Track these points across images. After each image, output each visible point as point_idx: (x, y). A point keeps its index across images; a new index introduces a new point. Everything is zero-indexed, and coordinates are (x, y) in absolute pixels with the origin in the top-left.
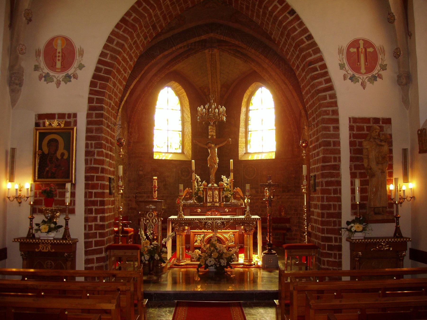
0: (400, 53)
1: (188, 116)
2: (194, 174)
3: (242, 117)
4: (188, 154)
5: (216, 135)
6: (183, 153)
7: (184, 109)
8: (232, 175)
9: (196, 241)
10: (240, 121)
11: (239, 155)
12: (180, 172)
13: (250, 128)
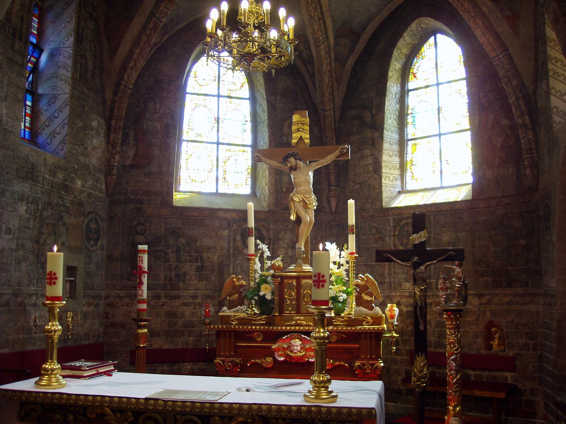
2: (252, 241)
3: (391, 106)
4: (262, 197)
5: (311, 138)
7: (258, 95)
8: (352, 238)
10: (384, 113)
11: (384, 195)
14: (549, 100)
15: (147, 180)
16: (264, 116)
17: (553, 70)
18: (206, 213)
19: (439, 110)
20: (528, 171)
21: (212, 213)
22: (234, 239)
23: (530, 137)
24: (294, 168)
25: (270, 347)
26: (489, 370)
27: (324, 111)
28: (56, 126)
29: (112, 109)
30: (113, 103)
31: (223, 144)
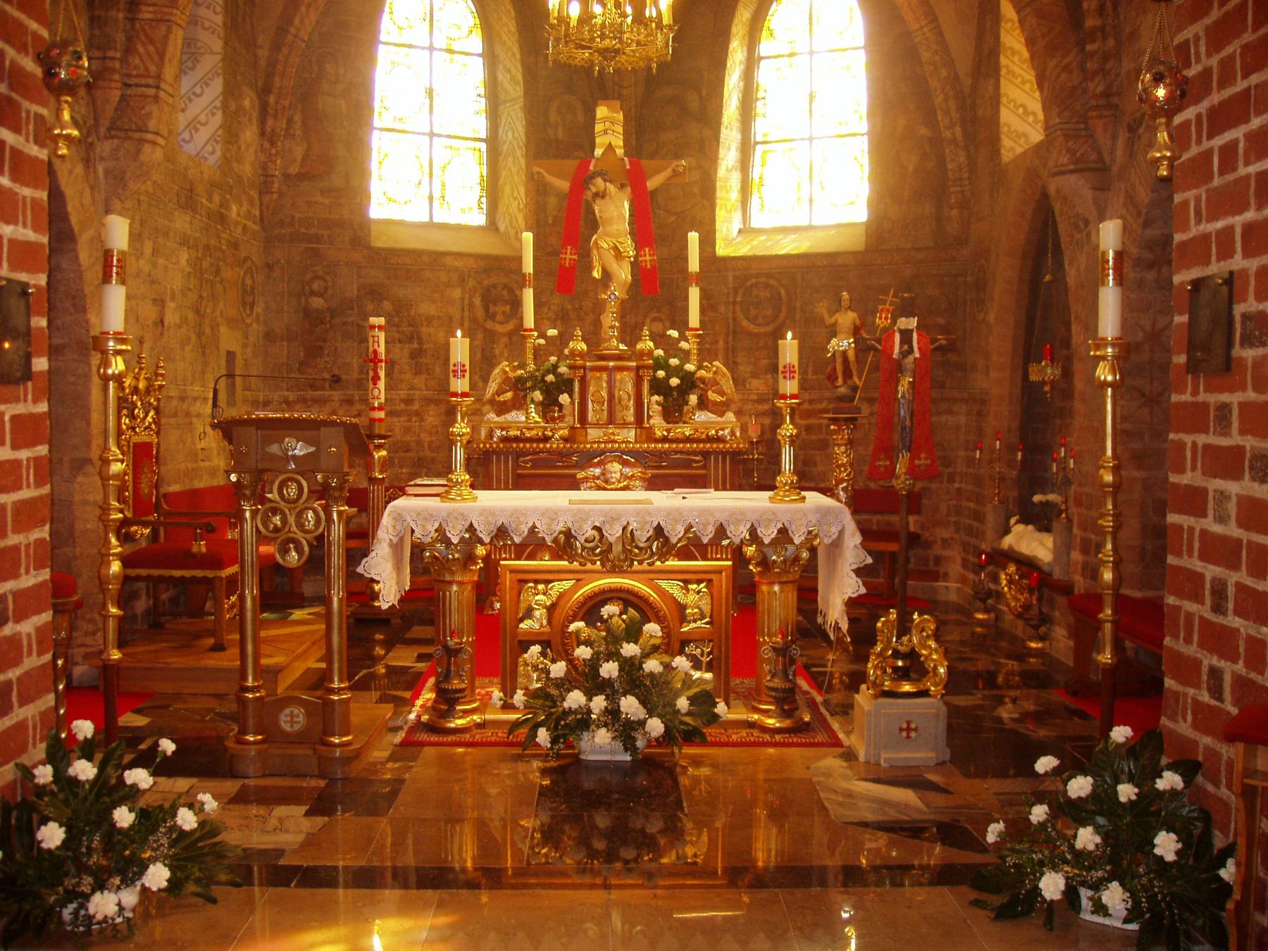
0: (210, 710)
1: (513, 79)
5: (625, 146)
6: (492, 224)
7: (499, 50)
9: (529, 613)
12: (477, 301)
13: (760, 129)
14: (998, 112)
15: (326, 201)
16: (514, 90)
17: (1007, 67)
18: (425, 258)
19: (812, 97)
20: (955, 212)
21: (436, 258)
22: (471, 305)
23: (961, 160)
24: (601, 195)
25: (574, 476)
26: (881, 512)
27: (621, 87)
28: (198, 111)
29: (270, 75)
30: (272, 64)
31: (439, 136)
